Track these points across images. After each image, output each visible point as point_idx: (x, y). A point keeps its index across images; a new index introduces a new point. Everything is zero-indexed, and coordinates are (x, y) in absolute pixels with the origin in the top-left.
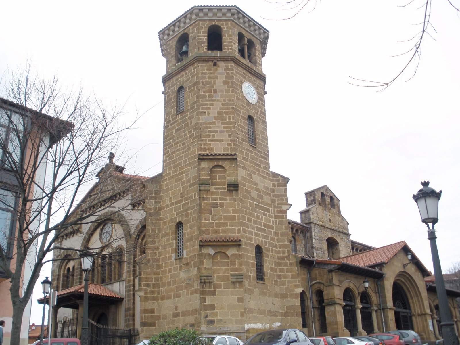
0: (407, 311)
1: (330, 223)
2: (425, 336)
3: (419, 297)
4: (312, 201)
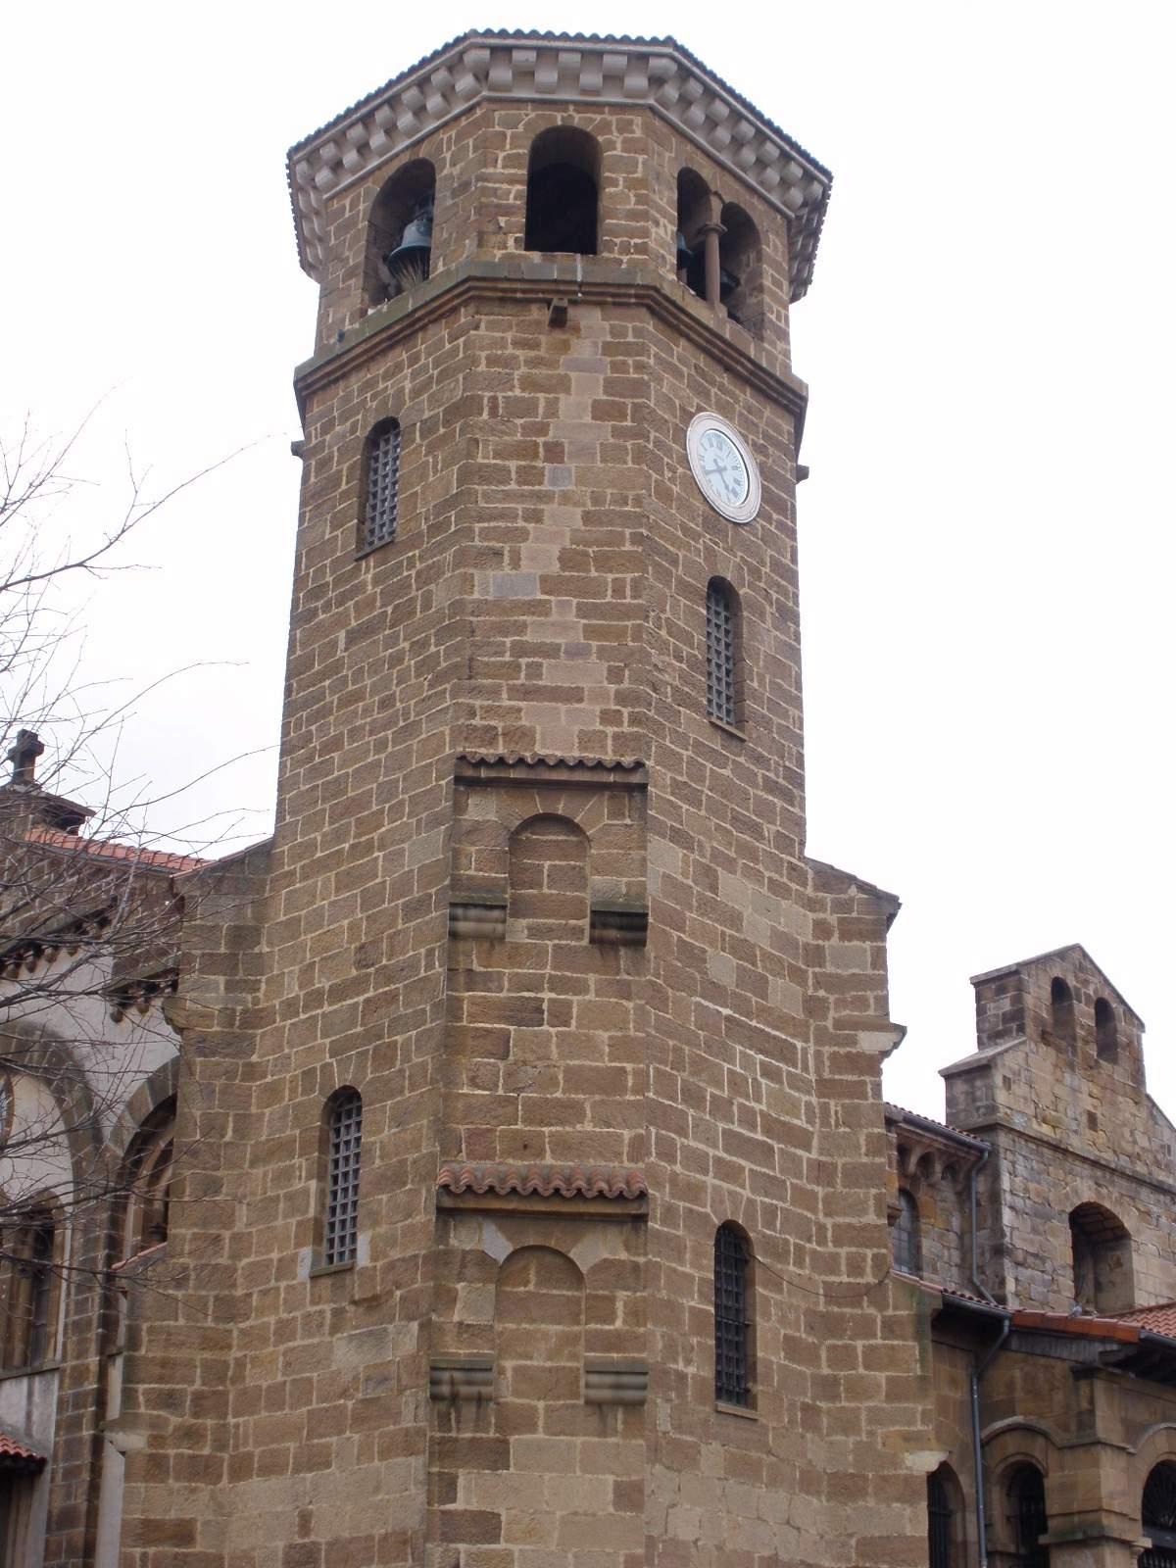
1: (1089, 1134)
4: (1007, 1018)
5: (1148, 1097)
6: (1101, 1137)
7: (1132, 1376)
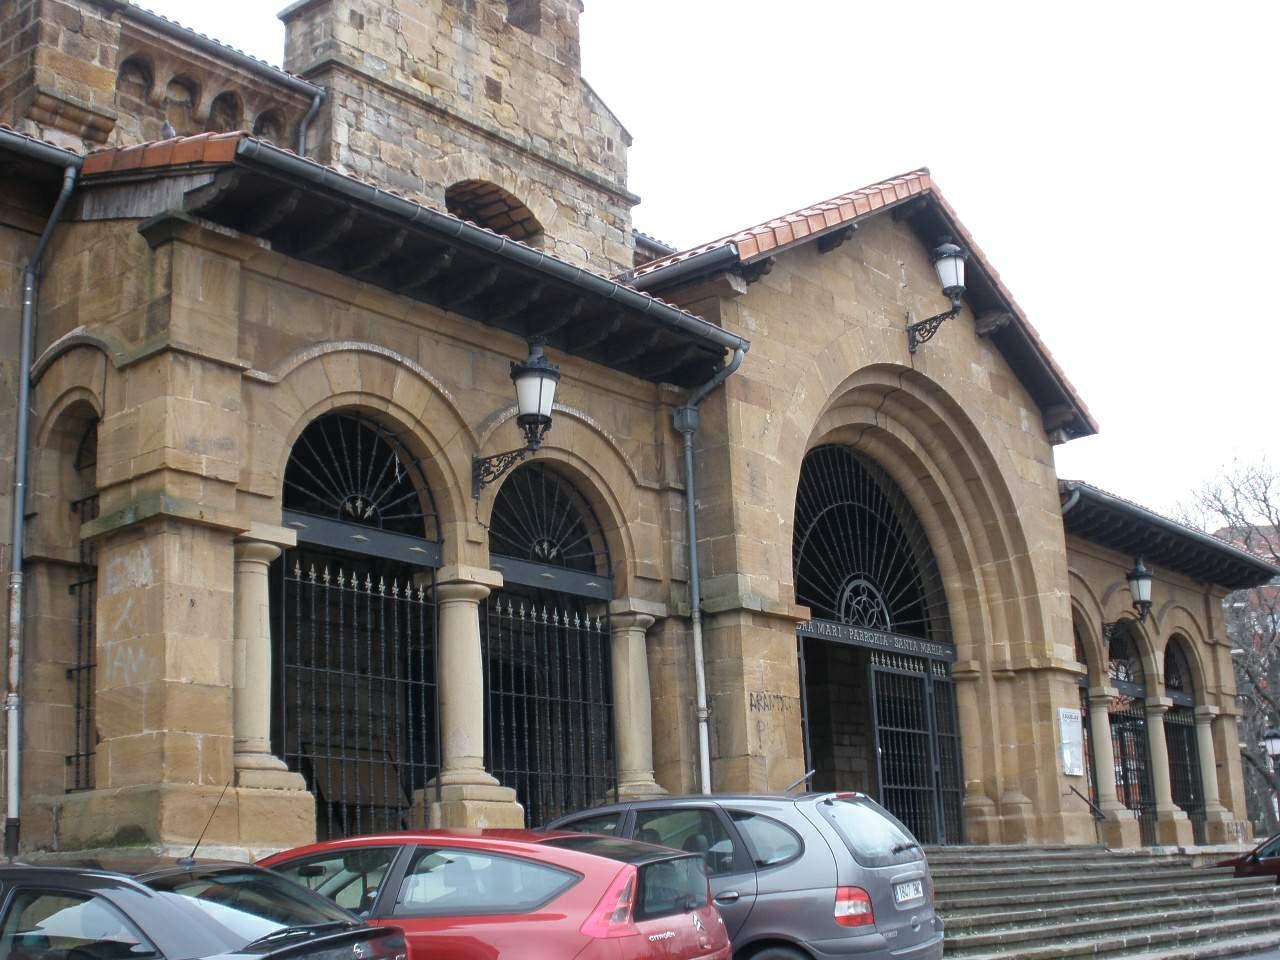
0: (928, 649)
1: (488, 104)
2: (1027, 815)
5: (583, 81)
6: (505, 111)
7: (265, 245)
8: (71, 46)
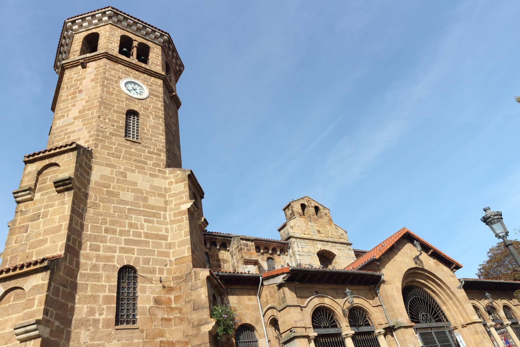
3: (454, 299)
4: (291, 214)
7: (297, 283)
8: (247, 250)
